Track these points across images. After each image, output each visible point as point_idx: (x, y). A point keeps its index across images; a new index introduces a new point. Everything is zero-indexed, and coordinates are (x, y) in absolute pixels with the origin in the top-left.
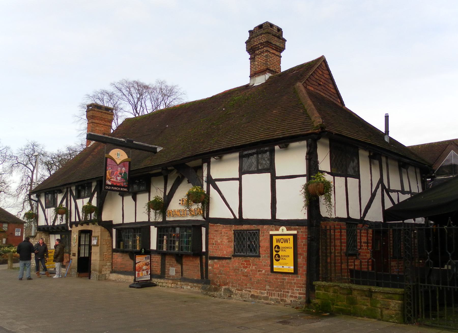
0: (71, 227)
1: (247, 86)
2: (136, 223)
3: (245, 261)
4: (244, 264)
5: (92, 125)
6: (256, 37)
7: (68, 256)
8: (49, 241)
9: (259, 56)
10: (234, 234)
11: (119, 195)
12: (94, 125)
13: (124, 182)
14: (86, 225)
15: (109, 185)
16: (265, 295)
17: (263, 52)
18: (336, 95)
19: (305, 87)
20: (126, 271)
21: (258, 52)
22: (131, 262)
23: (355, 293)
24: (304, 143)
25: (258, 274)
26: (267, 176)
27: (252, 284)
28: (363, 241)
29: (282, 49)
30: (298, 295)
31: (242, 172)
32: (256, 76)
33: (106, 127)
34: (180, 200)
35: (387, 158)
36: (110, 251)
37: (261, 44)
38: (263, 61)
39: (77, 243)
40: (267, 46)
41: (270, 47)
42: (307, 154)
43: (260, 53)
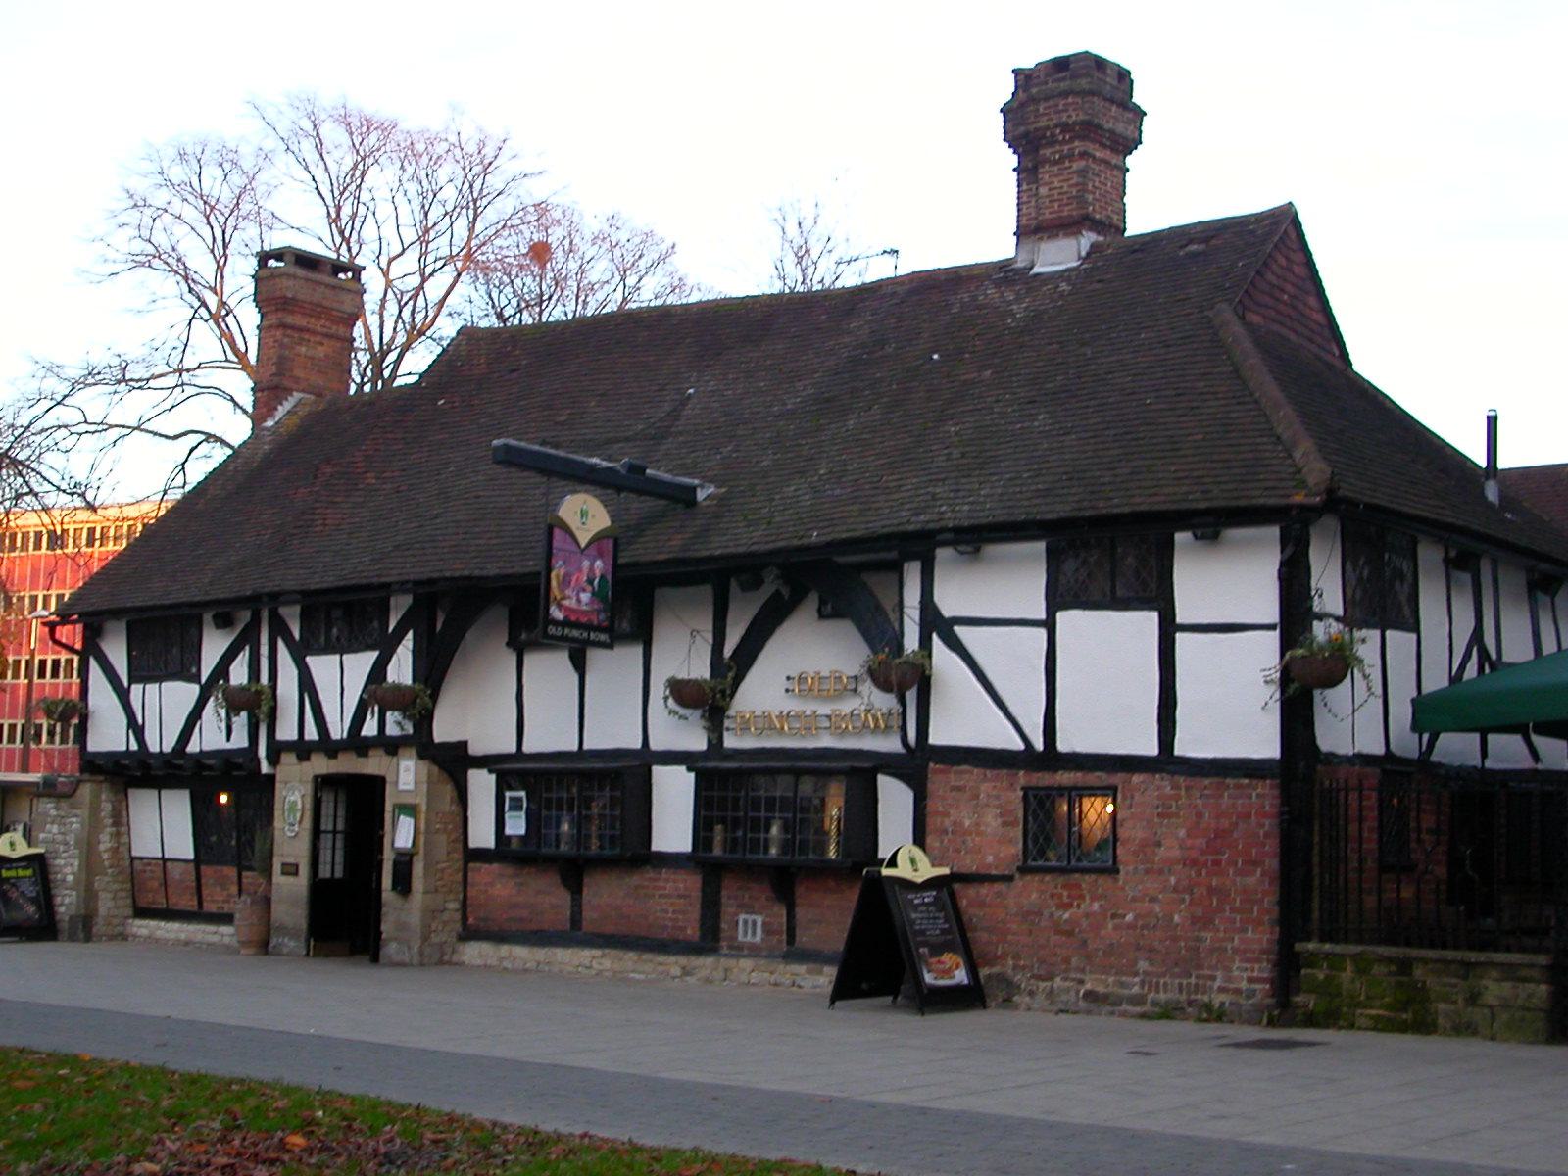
0: (274, 759)
1: (1003, 266)
2: (581, 753)
3: (1064, 887)
4: (1061, 896)
5: (285, 335)
6: (1046, 99)
7: (236, 875)
8: (125, 813)
9: (1056, 168)
10: (1025, 798)
11: (508, 644)
12: (288, 336)
13: (599, 611)
14: (326, 759)
15: (556, 623)
16: (1136, 989)
17: (1071, 157)
18: (1326, 333)
19: (1239, 318)
20: (536, 932)
21: (1052, 153)
22: (562, 898)
23: (1418, 972)
24: (1274, 532)
25: (1110, 926)
26: (1148, 621)
27: (1088, 957)
28: (1424, 826)
29: (1132, 143)
30: (1244, 985)
31: (1057, 600)
32: (1041, 239)
33: (333, 343)
34: (788, 678)
35: (1495, 562)
36: (458, 855)
37: (1065, 128)
38: (1070, 186)
39: (307, 823)
40: (1083, 138)
41: (1093, 141)
42: (1282, 564)
43: (1057, 156)
